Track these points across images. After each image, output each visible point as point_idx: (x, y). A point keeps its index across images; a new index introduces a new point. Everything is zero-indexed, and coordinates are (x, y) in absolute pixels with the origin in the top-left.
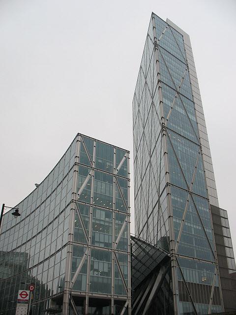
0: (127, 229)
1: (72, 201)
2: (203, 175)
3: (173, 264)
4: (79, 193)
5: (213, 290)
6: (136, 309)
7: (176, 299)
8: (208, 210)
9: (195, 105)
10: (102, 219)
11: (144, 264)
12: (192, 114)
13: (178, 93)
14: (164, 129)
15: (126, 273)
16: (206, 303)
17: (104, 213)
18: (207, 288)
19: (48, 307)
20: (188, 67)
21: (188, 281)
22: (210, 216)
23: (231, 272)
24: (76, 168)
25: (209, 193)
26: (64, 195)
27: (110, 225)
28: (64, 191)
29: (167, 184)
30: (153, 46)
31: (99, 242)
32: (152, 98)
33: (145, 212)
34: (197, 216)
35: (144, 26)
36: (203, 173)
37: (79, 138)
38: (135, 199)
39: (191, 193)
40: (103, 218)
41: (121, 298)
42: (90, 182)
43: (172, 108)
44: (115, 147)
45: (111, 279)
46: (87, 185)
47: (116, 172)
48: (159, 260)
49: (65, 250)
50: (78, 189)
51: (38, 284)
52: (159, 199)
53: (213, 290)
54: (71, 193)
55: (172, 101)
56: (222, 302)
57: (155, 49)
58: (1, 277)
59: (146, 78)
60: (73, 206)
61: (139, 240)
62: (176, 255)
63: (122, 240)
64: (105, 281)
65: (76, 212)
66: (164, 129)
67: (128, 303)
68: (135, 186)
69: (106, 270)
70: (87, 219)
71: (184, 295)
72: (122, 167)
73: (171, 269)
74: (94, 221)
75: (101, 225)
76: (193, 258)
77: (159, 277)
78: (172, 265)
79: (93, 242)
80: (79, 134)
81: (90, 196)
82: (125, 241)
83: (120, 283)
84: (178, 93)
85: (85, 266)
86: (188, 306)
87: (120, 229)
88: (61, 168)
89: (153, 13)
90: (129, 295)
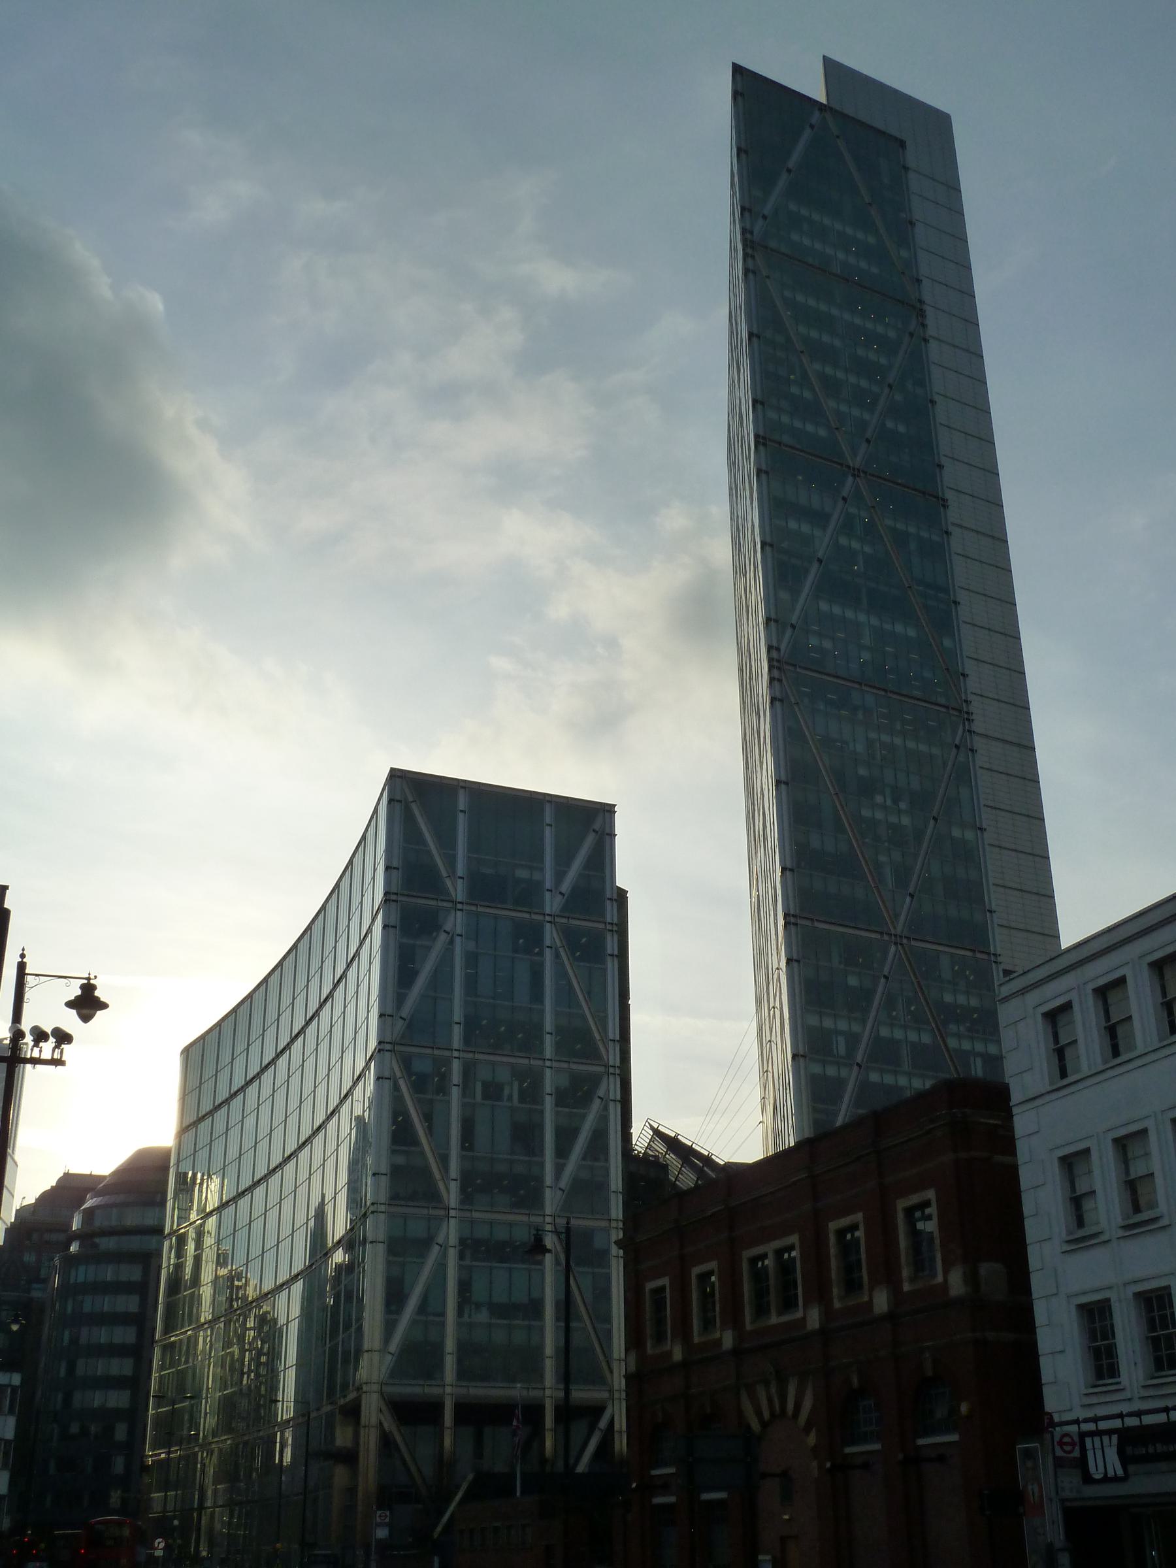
65: (396, 1088)
67: (618, 1414)
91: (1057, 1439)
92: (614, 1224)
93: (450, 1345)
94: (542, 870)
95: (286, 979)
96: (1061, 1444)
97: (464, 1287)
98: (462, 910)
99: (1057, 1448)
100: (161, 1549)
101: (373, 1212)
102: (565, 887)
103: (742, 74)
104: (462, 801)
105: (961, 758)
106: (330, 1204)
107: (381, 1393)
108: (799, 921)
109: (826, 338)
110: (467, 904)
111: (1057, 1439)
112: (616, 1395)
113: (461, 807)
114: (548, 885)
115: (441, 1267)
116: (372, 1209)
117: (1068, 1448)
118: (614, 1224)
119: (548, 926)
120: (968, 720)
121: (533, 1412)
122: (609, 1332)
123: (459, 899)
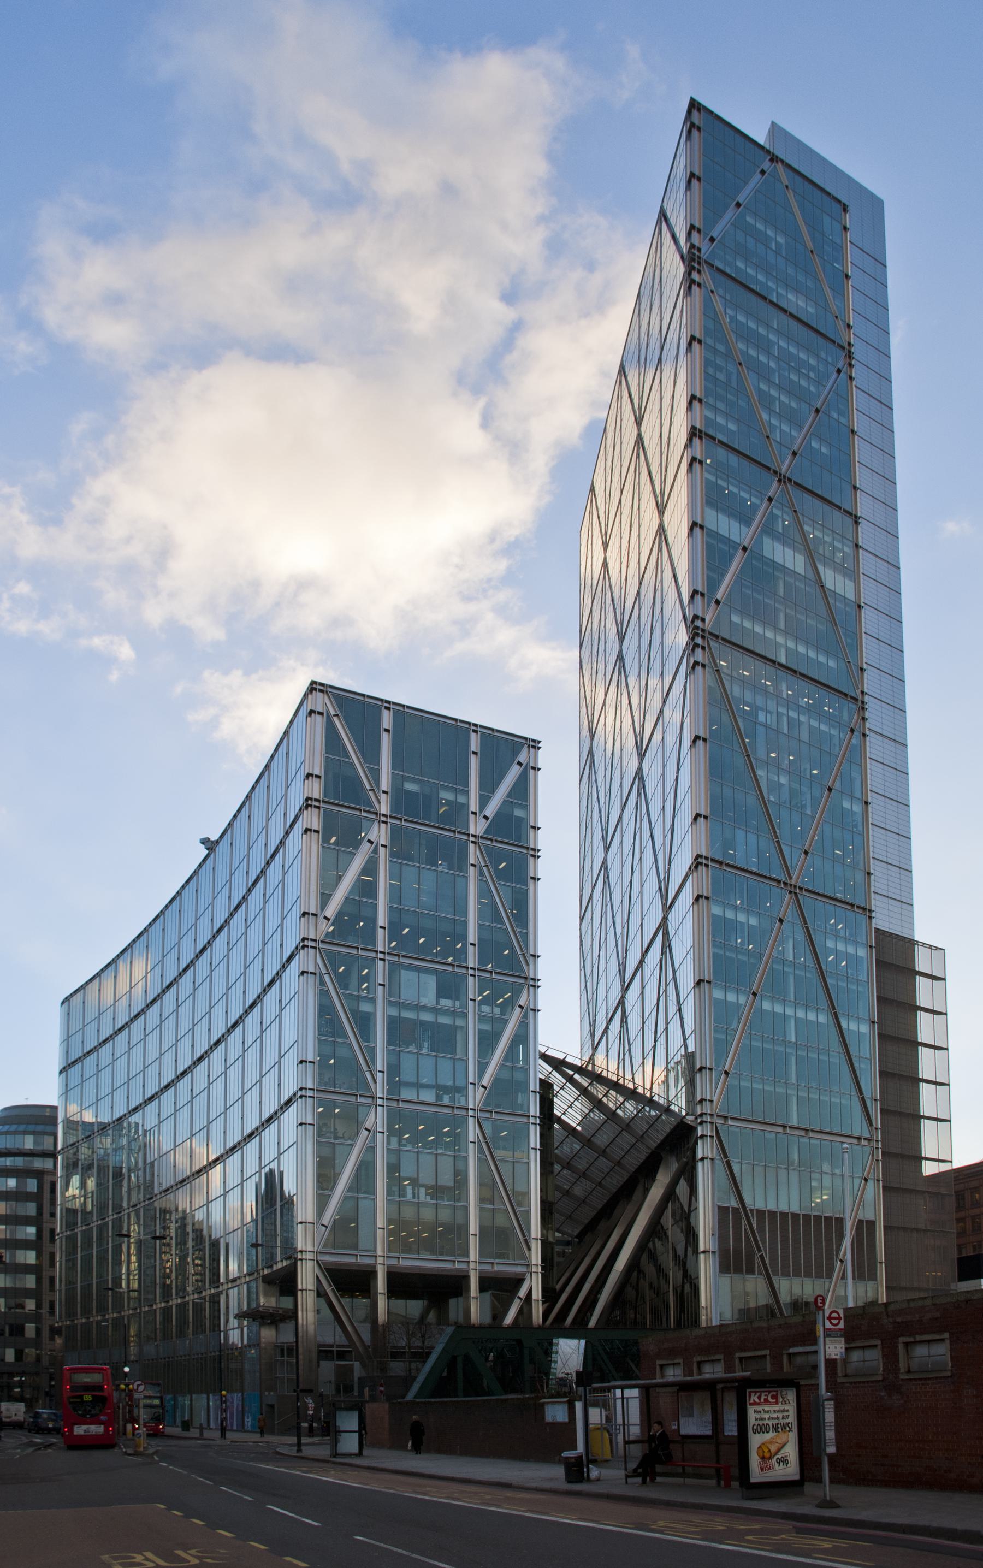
1: (304, 944)
2: (859, 818)
4: (331, 911)
7: (706, 1269)
8: (862, 952)
10: (424, 1001)
11: (603, 1153)
12: (838, 568)
14: (699, 640)
15: (520, 1188)
16: (820, 1275)
17: (431, 983)
19: (249, 1304)
21: (760, 1205)
22: (867, 973)
23: (929, 1169)
24: (313, 819)
25: (877, 883)
26: (273, 920)
27: (459, 1022)
28: (274, 907)
29: (698, 862)
30: (682, 269)
31: (418, 1086)
32: (661, 509)
33: (614, 967)
34: (812, 975)
35: (768, 126)
36: (857, 808)
37: (319, 701)
38: (582, 919)
39: (795, 891)
40: (429, 998)
41: (501, 1268)
42: (370, 868)
43: (745, 549)
44: (476, 728)
45: (466, 1209)
46: (359, 880)
47: (477, 827)
48: (657, 1137)
49: (290, 1117)
50: (325, 899)
52: (665, 919)
54: (296, 913)
55: (745, 518)
56: (882, 1271)
57: (689, 284)
59: (639, 421)
60: (307, 960)
61: (598, 1078)
63: (506, 1075)
64: (445, 1215)
65: (322, 982)
66: (699, 640)
67: (534, 1285)
68: (582, 869)
69: (447, 1179)
70: (365, 1007)
71: (737, 1251)
72: (507, 803)
73: (694, 1168)
74: (394, 1012)
75: (423, 1024)
76: (784, 1127)
77: (656, 1192)
78: (700, 1155)
79: (394, 1086)
80: (314, 687)
81: (374, 920)
82: (519, 1076)
83: (500, 1221)
85: (365, 1170)
86: (750, 1286)
87: (497, 1036)
89: (694, 105)
90: (536, 1256)
91: (827, 1315)
92: (532, 1120)
93: (473, 1228)
94: (467, 793)
96: (830, 1318)
97: (393, 1169)
99: (827, 1322)
101: (301, 1097)
102: (490, 810)
103: (699, 110)
104: (474, 742)
105: (854, 741)
107: (317, 1261)
108: (710, 863)
109: (763, 358)
110: (391, 817)
112: (534, 1269)
113: (473, 748)
114: (473, 808)
115: (371, 1149)
116: (300, 1093)
117: (835, 1322)
118: (532, 1120)
119: (472, 846)
121: (457, 1284)
122: (528, 1213)
123: (383, 811)
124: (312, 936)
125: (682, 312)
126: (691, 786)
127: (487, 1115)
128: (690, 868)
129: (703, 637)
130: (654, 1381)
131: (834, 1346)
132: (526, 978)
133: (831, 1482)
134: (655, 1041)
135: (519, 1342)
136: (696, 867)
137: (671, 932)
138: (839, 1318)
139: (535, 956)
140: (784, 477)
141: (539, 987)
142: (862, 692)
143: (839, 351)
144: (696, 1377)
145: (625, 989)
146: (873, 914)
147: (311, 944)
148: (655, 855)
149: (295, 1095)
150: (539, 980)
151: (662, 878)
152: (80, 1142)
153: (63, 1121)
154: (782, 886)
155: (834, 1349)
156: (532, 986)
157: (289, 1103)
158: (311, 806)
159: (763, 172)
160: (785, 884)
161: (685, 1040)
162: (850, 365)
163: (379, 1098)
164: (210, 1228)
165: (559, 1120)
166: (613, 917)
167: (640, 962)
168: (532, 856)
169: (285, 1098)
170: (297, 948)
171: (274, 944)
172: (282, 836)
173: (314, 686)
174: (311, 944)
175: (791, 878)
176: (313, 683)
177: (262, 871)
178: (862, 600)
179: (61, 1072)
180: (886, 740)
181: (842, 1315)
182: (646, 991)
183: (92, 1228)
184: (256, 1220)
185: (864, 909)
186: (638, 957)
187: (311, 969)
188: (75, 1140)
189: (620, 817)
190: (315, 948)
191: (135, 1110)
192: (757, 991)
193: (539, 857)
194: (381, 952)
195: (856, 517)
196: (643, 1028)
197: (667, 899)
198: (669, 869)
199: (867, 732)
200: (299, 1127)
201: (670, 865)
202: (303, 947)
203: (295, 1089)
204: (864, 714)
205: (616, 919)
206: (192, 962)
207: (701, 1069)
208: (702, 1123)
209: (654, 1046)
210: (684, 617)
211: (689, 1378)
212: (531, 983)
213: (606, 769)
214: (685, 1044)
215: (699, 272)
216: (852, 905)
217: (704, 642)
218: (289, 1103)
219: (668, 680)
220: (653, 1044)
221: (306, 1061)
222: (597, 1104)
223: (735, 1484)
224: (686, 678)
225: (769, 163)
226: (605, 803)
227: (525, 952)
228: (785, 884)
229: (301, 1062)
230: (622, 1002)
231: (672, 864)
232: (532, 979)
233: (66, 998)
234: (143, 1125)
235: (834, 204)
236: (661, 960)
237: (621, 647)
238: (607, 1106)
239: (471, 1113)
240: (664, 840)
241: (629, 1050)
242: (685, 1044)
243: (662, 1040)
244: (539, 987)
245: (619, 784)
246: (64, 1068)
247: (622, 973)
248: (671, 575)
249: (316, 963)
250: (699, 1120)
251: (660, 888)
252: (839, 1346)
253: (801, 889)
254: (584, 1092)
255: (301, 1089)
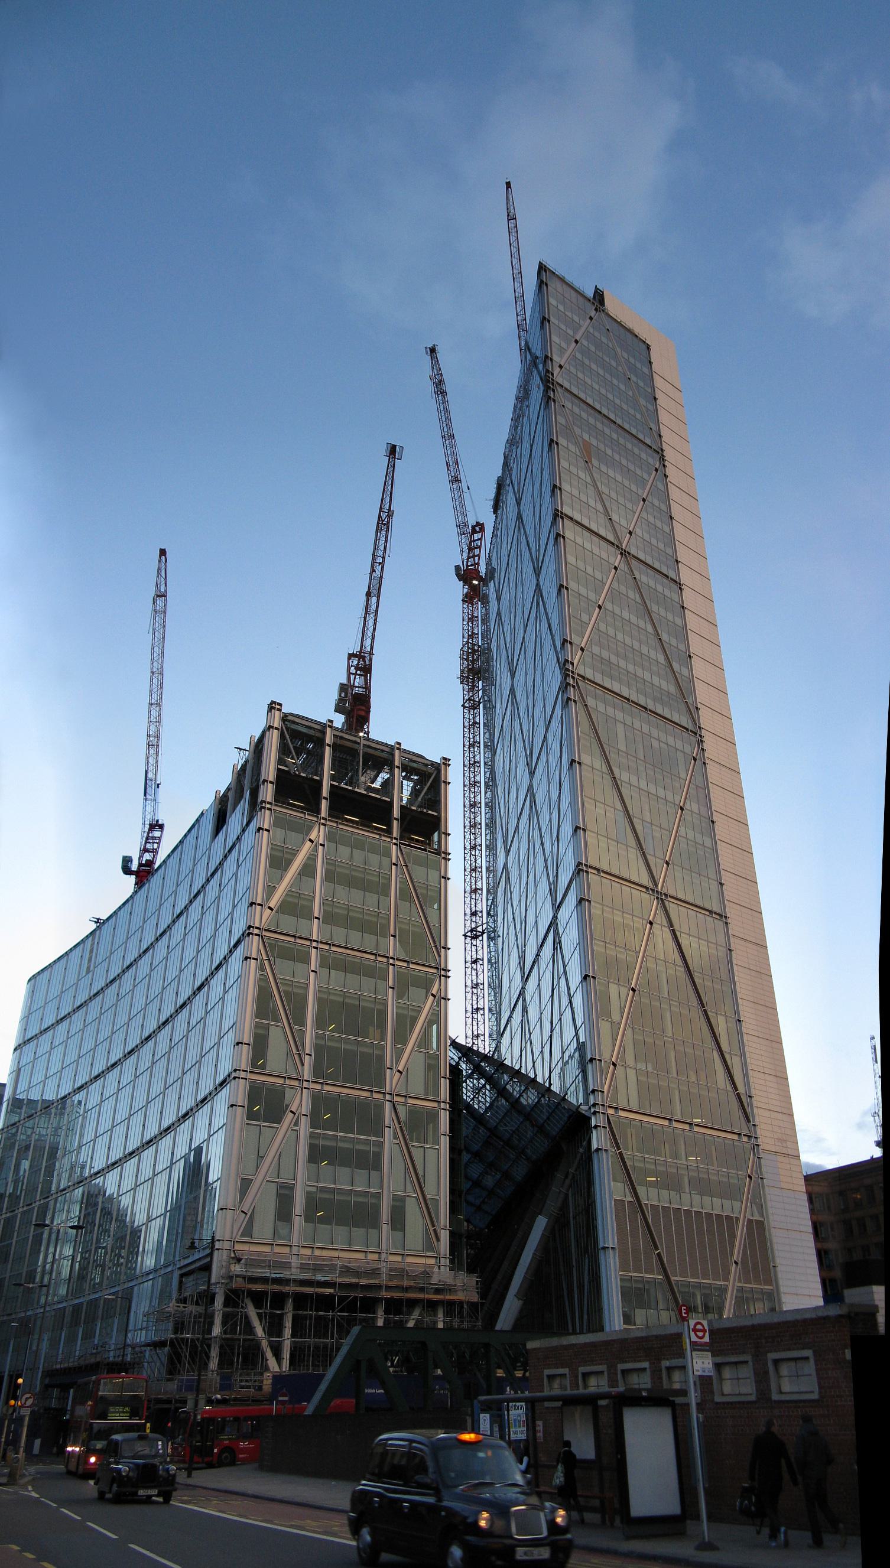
0: (438, 1018)
1: (247, 933)
3: (598, 1139)
5: (741, 1231)
6: (419, 1448)
9: (686, 592)
13: (624, 554)
18: (720, 1224)
20: (662, 459)
32: (537, 572)
49: (222, 1100)
50: (270, 891)
51: (121, 1221)
52: (555, 917)
53: (741, 1231)
54: (245, 903)
55: (643, 483)
58: (2, 1191)
60: (254, 945)
62: (611, 1111)
73: (590, 1159)
84: (624, 554)
88: (187, 865)
91: (691, 1327)
95: (167, 996)
98: (316, 948)
99: (692, 1334)
100: (28, 1407)
101: (235, 1078)
106: (179, 1157)
108: (590, 870)
111: (691, 1327)
116: (234, 1075)
117: (700, 1334)
120: (701, 741)
124: (257, 925)
125: (543, 420)
126: (570, 802)
127: (402, 1100)
128: (573, 874)
129: (573, 678)
130: (538, 1394)
131: (701, 1361)
132: (438, 969)
133: (710, 1518)
134: (552, 1031)
135: (424, 1344)
136: (578, 873)
137: (561, 930)
138: (704, 1331)
139: (446, 948)
140: (625, 551)
141: (449, 977)
142: (700, 728)
143: (655, 455)
144: (581, 1391)
145: (525, 980)
146: (729, 921)
147: (256, 931)
148: (546, 861)
149: (229, 1076)
150: (449, 971)
151: (552, 881)
152: (22, 1122)
153: (8, 1100)
154: (651, 892)
155: (701, 1364)
156: (443, 976)
157: (223, 1083)
158: (264, 808)
159: (591, 318)
160: (653, 890)
161: (577, 1031)
162: (664, 466)
163: (306, 1081)
164: (133, 1215)
165: (469, 1107)
166: (513, 914)
167: (536, 956)
168: (444, 858)
169: (220, 1078)
170: (243, 935)
171: (224, 931)
172: (239, 833)
173: (274, 705)
174: (256, 931)
175: (656, 885)
176: (273, 702)
177: (220, 864)
178: (691, 651)
179: (15, 1050)
180: (724, 769)
181: (706, 1328)
182: (542, 982)
183: (34, 1208)
184: (180, 1207)
185: (721, 915)
186: (534, 951)
187: (254, 955)
188: (17, 1119)
189: (517, 826)
190: (259, 935)
191: (81, 1088)
192: (636, 987)
193: (449, 859)
194: (315, 941)
195: (680, 584)
196: (540, 1018)
197: (556, 900)
198: (557, 873)
199: (707, 761)
200: (230, 1109)
201: (557, 870)
202: (249, 934)
203: (230, 1070)
204: (703, 746)
205: (516, 915)
206: (152, 944)
207: (591, 1060)
208: (595, 1113)
209: (551, 1036)
210: (558, 660)
211: (576, 1392)
212: (443, 973)
213: (505, 784)
214: (577, 1035)
215: (553, 391)
216: (710, 912)
217: (574, 682)
218: (223, 1083)
219: (504, 707)
220: (550, 1034)
221: (242, 1043)
222: (501, 1092)
223: (618, 1521)
224: (562, 711)
225: (594, 312)
226: (505, 813)
227: (438, 944)
228: (653, 890)
229: (238, 1043)
230: (522, 993)
231: (559, 870)
232: (443, 969)
233: (34, 976)
234: (85, 1104)
235: (641, 344)
236: (553, 955)
237: (512, 682)
238: (511, 1095)
239: (388, 1097)
240: (552, 849)
241: (530, 1038)
242: (577, 1035)
243: (557, 1029)
244: (449, 977)
245: (515, 797)
246: (19, 1045)
247: (522, 965)
248: (547, 625)
249: (259, 951)
250: (592, 1110)
251: (550, 890)
252: (706, 1362)
253: (666, 895)
254: (489, 1079)
255: (235, 1070)
